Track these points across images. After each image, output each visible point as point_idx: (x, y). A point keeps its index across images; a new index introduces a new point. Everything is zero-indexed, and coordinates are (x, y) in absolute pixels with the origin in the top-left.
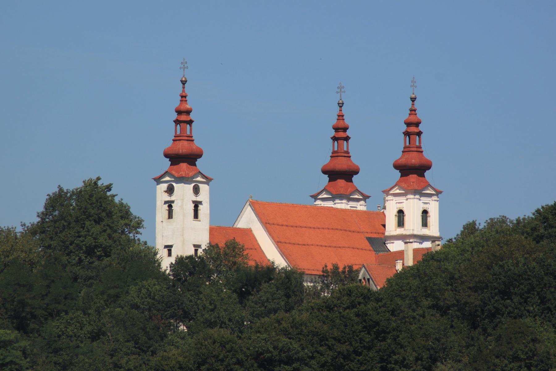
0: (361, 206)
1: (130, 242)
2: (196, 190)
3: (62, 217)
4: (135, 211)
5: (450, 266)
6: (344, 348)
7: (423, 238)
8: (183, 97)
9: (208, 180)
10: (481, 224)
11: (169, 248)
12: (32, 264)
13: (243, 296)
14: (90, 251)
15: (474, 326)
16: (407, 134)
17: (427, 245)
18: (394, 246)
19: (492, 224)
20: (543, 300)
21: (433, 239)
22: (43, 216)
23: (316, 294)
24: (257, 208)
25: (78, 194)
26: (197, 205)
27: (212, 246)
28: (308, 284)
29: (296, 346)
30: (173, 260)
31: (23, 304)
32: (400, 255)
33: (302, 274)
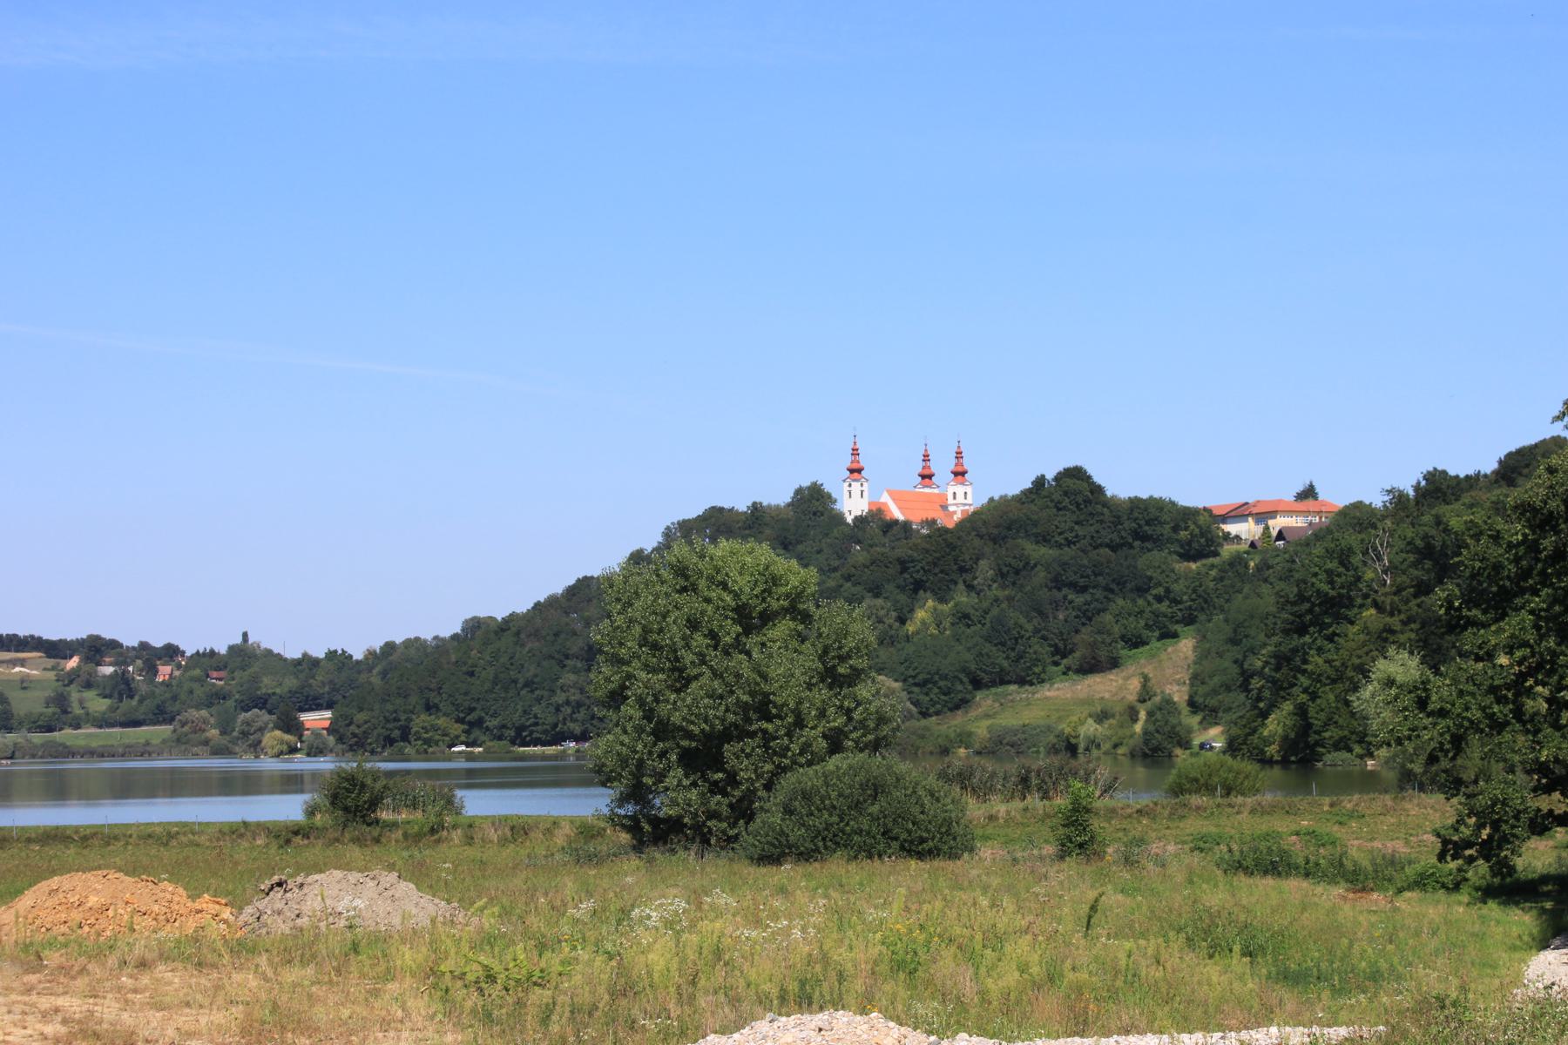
0: (936, 491)
1: (833, 509)
2: (862, 485)
3: (801, 499)
4: (834, 495)
5: (983, 517)
6: (937, 555)
7: (965, 505)
8: (855, 443)
9: (867, 480)
10: (996, 498)
11: (850, 512)
12: (789, 520)
13: (885, 533)
14: (815, 514)
15: (995, 544)
16: (957, 457)
17: (967, 507)
18: (951, 509)
19: (1001, 497)
20: (1026, 532)
21: (970, 505)
22: (793, 498)
23: (918, 531)
24: (891, 493)
25: (809, 488)
26: (862, 492)
27: (870, 511)
28: (914, 527)
29: (915, 555)
30: (852, 517)
31: (786, 538)
32: (955, 512)
33: (911, 522)
